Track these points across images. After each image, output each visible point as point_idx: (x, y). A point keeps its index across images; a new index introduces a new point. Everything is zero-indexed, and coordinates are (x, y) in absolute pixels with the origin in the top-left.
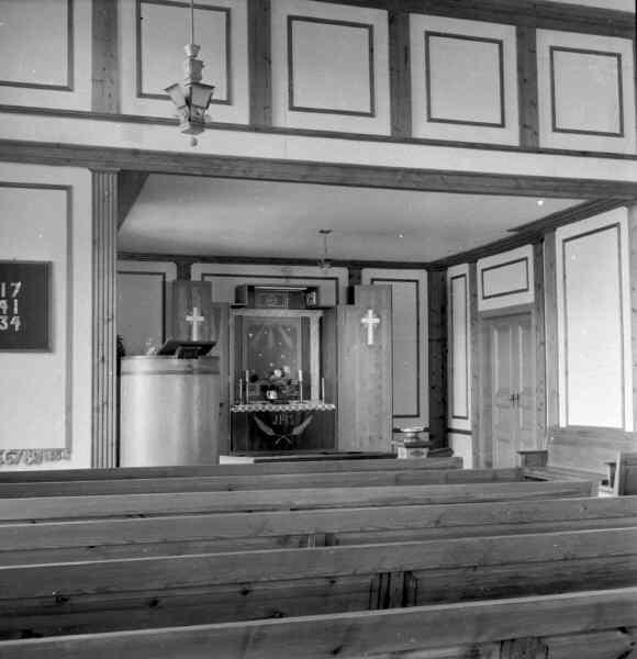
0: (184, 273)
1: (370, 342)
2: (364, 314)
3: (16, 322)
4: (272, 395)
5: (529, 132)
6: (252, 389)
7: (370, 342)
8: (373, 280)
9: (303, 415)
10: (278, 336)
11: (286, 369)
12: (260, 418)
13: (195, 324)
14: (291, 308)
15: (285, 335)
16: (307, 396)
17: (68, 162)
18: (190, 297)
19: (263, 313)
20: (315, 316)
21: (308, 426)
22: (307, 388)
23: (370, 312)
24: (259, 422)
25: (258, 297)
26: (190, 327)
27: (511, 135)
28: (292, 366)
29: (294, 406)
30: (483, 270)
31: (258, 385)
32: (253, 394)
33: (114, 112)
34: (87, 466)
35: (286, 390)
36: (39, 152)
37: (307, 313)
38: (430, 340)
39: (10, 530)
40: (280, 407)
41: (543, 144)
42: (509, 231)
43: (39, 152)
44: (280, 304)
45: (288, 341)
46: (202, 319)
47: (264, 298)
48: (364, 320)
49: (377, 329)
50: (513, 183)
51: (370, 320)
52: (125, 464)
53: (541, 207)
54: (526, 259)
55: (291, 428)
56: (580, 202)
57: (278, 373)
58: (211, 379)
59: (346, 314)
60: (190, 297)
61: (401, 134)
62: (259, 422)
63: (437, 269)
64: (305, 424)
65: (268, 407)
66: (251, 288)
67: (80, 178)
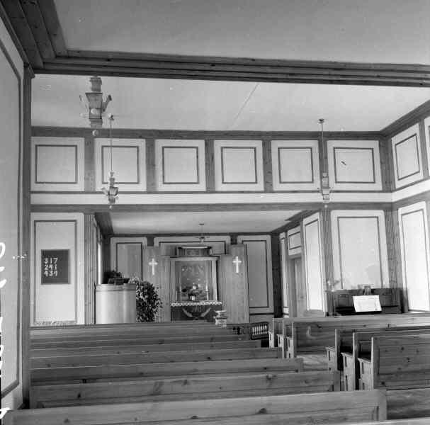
0: (151, 243)
1: (237, 271)
2: (235, 258)
3: (56, 272)
4: (193, 298)
5: (268, 185)
6: (184, 295)
7: (237, 271)
8: (243, 241)
9: (206, 307)
10: (196, 270)
11: (199, 286)
12: (186, 309)
13: (153, 266)
14: (202, 256)
15: (200, 270)
16: (211, 298)
17: (75, 211)
18: (151, 254)
19: (193, 259)
20: (213, 260)
21: (208, 314)
22: (211, 294)
23: (237, 257)
24: (185, 312)
25: (186, 253)
26: (151, 267)
27: (260, 186)
28: (204, 285)
29: (202, 303)
30: (403, 215)
31: (186, 293)
32: (184, 298)
33: (92, 190)
34: (83, 323)
35: (200, 295)
36: (59, 208)
37: (210, 259)
38: (273, 269)
39: (23, 294)
40: (195, 303)
41: (275, 189)
42: (286, 220)
43: (59, 208)
44: (197, 255)
45: (202, 272)
46: (156, 264)
47: (189, 253)
48: (234, 262)
49: (157, 268)
50: (261, 206)
51: (237, 261)
52: (98, 323)
53: (292, 213)
54: (422, 210)
55: (200, 314)
56: (300, 211)
57: (194, 288)
58: (132, 293)
59: (226, 261)
60: (151, 254)
61: (211, 190)
62: (185, 312)
63: (275, 235)
64: (207, 311)
65: (192, 304)
66: (180, 248)
67: (80, 217)
